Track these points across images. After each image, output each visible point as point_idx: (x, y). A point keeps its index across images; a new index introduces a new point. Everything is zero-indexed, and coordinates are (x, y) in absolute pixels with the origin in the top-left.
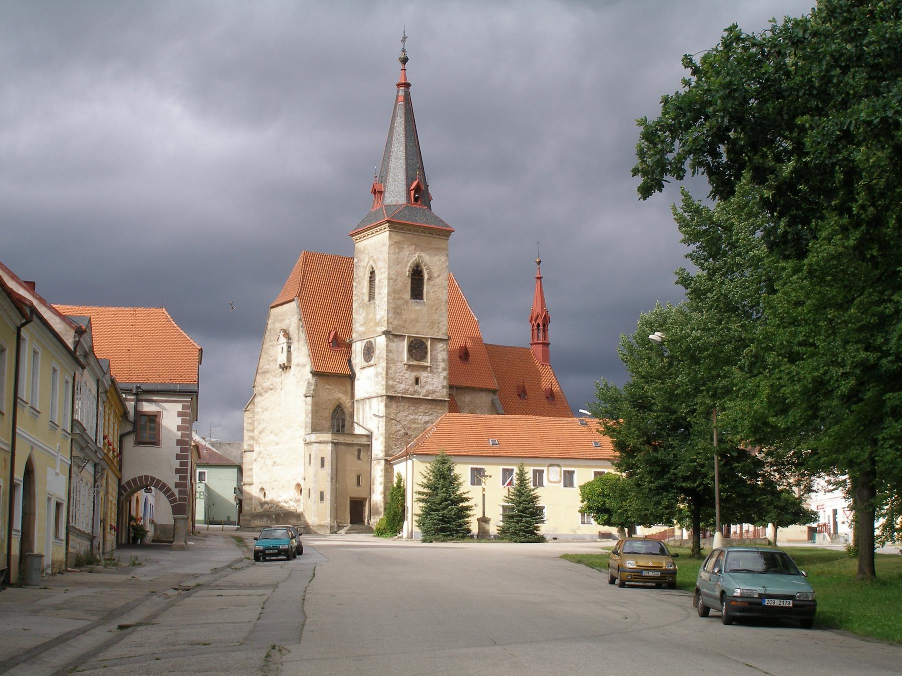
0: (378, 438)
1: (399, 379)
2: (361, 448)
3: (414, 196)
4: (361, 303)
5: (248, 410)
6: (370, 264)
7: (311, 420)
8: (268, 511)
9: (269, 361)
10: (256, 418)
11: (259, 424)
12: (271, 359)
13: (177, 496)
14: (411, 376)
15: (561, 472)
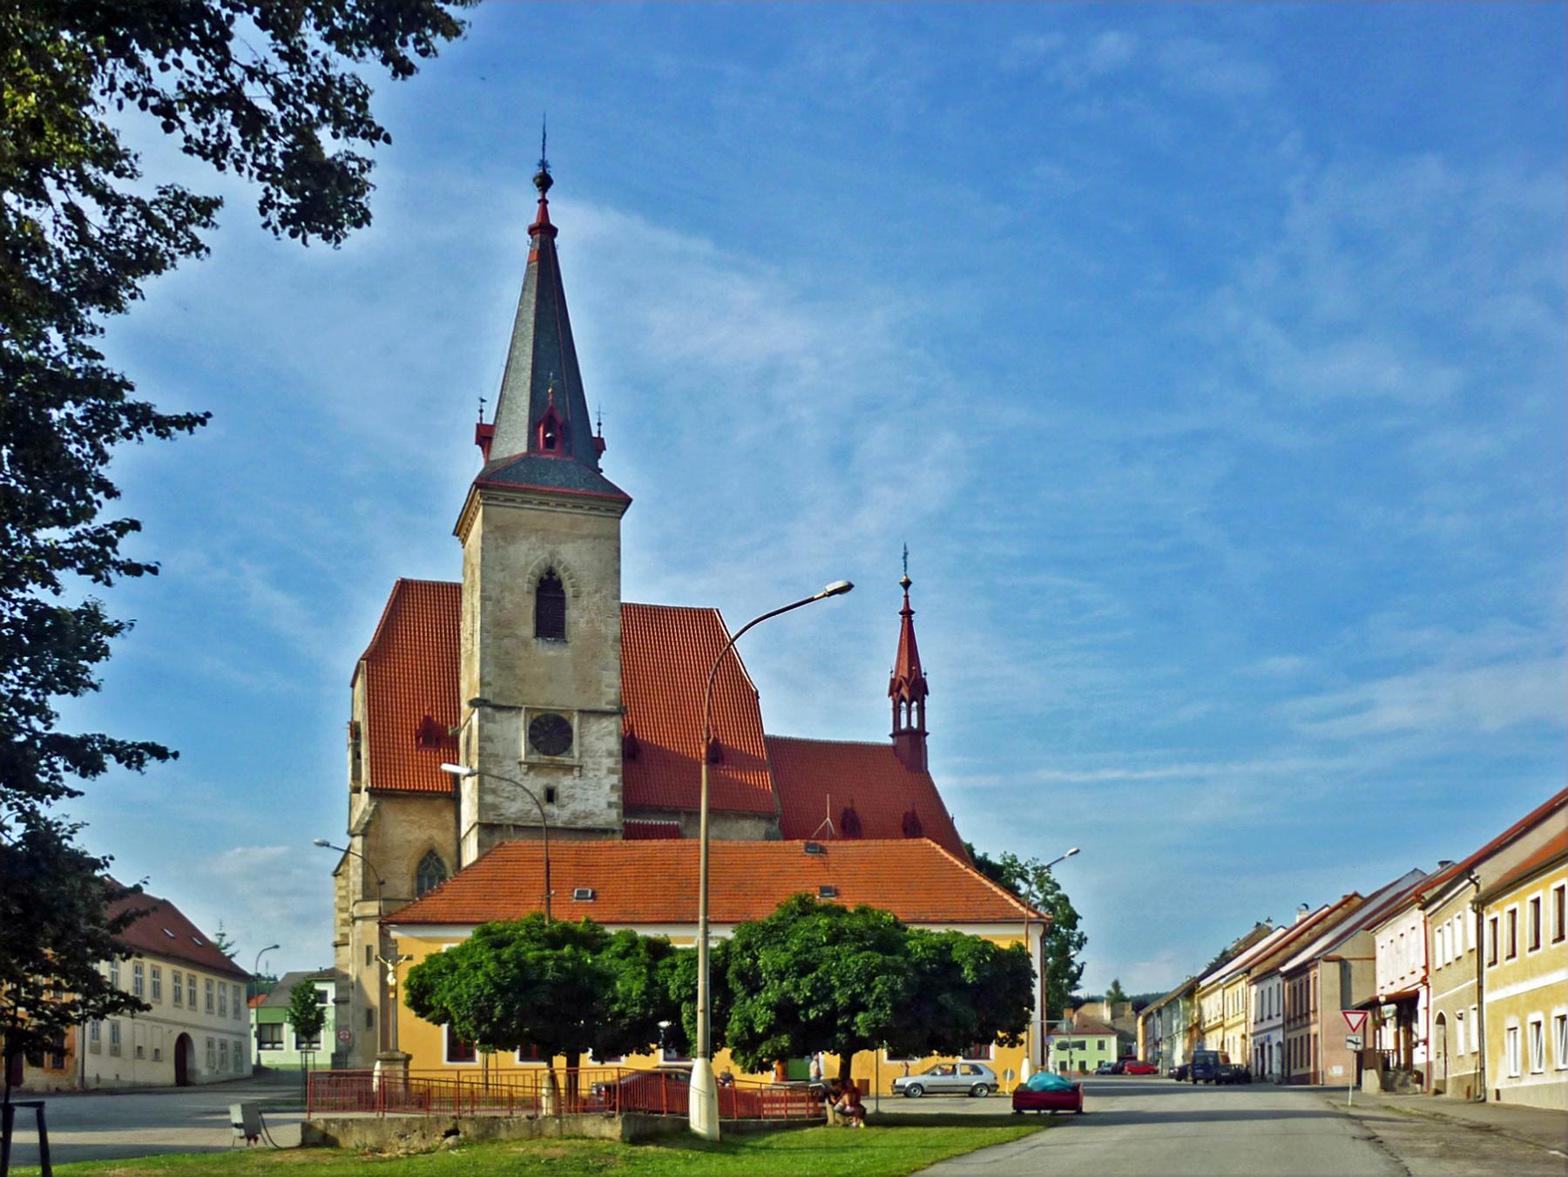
1: (509, 792)
3: (544, 435)
5: (340, 874)
7: (361, 879)
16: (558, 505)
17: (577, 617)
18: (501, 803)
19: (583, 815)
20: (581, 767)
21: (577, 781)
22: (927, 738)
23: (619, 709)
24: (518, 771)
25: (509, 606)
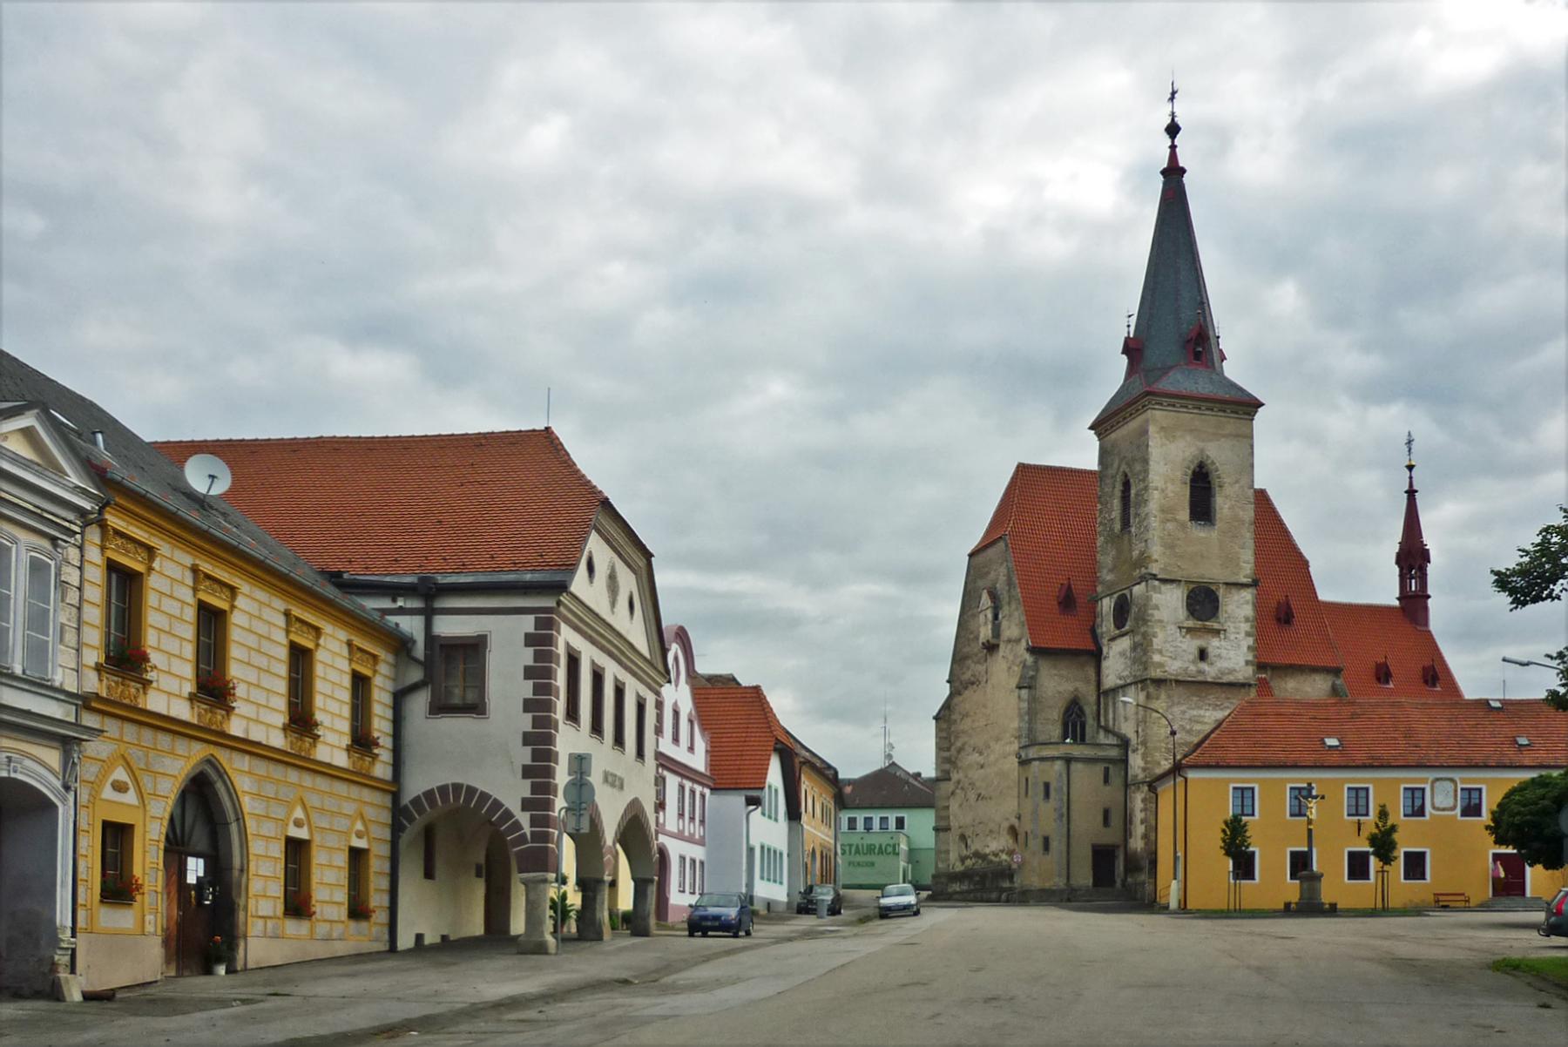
0: (1137, 749)
1: (1171, 652)
2: (1111, 766)
4: (1109, 536)
6: (1121, 470)
8: (972, 869)
9: (969, 640)
10: (952, 729)
11: (957, 737)
12: (972, 636)
13: (527, 829)
14: (1191, 645)
15: (1456, 791)
16: (1207, 409)
17: (1223, 504)
18: (1166, 661)
19: (1227, 671)
20: (1225, 630)
21: (1223, 643)
22: (1430, 601)
23: (1254, 581)
24: (1178, 634)
25: (1171, 495)
